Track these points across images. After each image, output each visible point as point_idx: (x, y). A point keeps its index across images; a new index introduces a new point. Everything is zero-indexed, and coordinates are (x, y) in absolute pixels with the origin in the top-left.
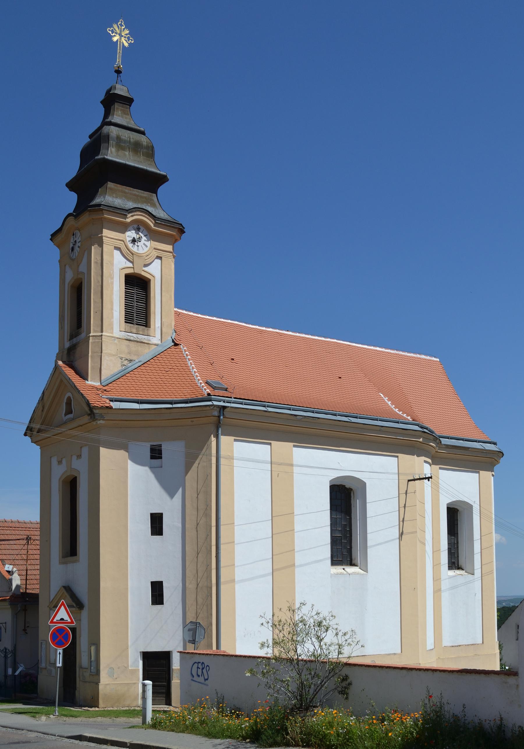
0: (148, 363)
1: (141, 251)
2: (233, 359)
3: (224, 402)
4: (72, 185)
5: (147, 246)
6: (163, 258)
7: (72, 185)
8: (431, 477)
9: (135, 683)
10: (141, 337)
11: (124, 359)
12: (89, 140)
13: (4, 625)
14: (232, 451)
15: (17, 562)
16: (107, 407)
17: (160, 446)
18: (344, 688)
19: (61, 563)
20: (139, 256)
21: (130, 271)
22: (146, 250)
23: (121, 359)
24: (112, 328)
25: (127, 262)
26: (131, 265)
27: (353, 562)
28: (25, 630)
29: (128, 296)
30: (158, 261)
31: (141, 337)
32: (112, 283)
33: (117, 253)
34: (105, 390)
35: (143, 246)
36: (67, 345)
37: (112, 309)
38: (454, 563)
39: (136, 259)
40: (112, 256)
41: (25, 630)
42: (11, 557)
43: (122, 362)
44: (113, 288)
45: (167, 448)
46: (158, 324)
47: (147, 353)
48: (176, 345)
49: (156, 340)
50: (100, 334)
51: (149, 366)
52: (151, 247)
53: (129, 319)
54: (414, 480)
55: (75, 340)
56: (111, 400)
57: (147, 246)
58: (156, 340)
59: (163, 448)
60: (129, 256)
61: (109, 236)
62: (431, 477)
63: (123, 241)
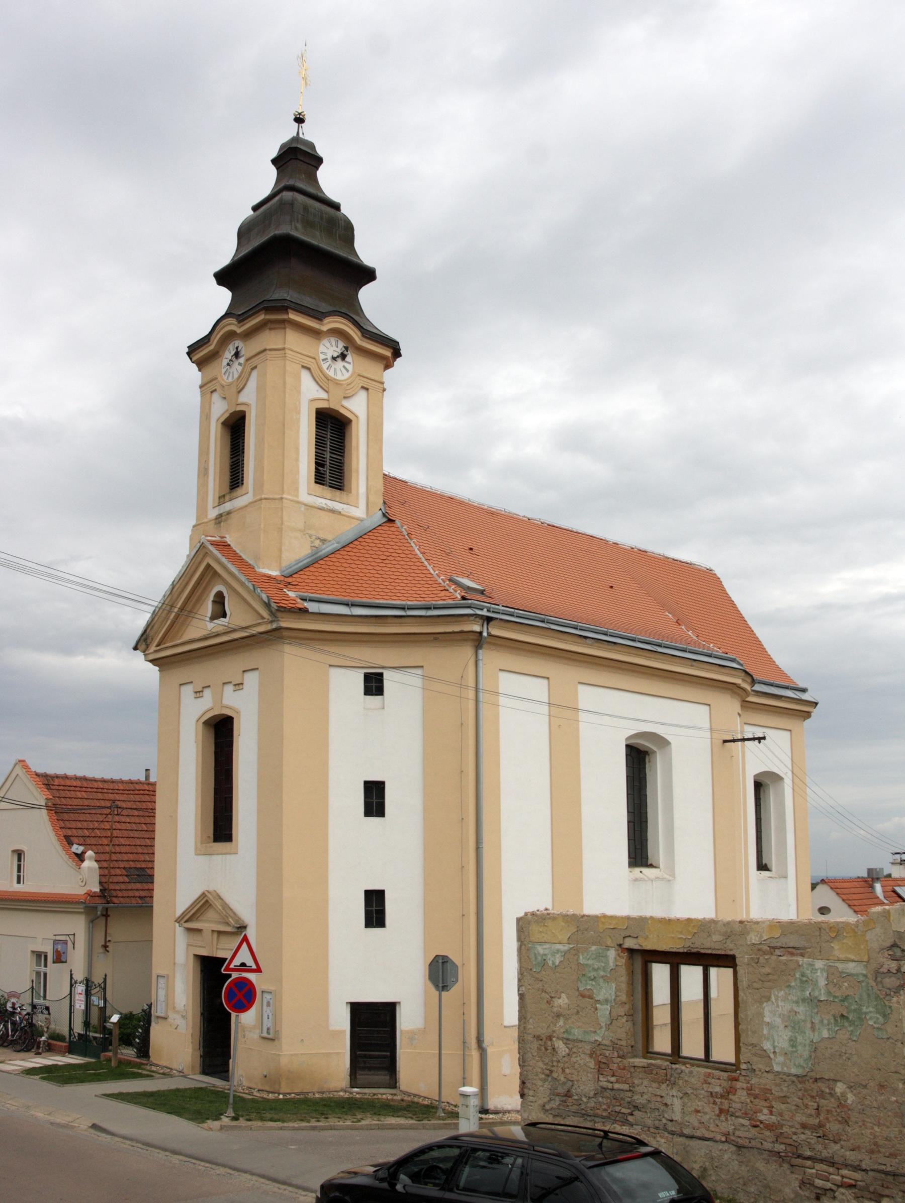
0: (351, 545)
1: (339, 377)
2: (471, 549)
3: (488, 611)
4: (223, 277)
5: (348, 371)
6: (370, 390)
7: (223, 277)
8: (764, 738)
9: (338, 1053)
10: (338, 506)
11: (314, 538)
12: (252, 213)
13: (72, 937)
14: (497, 688)
15: (88, 841)
16: (300, 609)
17: (381, 675)
18: (546, 1041)
19: (198, 853)
20: (337, 383)
21: (323, 405)
22: (347, 375)
23: (310, 537)
24: (297, 489)
25: (321, 390)
26: (324, 395)
27: (649, 862)
28: (105, 947)
29: (320, 443)
30: (363, 394)
31: (338, 506)
32: (298, 420)
33: (305, 376)
34: (289, 583)
35: (343, 370)
36: (213, 514)
37: (297, 460)
38: (762, 867)
39: (332, 387)
40: (298, 379)
41: (105, 947)
42: (80, 833)
43: (312, 542)
44: (299, 427)
45: (390, 680)
46: (362, 489)
47: (345, 531)
48: (390, 521)
49: (359, 512)
50: (279, 496)
51: (354, 550)
52: (354, 372)
53: (320, 479)
54: (734, 741)
55: (228, 506)
56: (304, 600)
57: (348, 371)
58: (359, 512)
59: (385, 676)
60: (324, 382)
61: (295, 349)
62: (764, 738)
63: (314, 358)
